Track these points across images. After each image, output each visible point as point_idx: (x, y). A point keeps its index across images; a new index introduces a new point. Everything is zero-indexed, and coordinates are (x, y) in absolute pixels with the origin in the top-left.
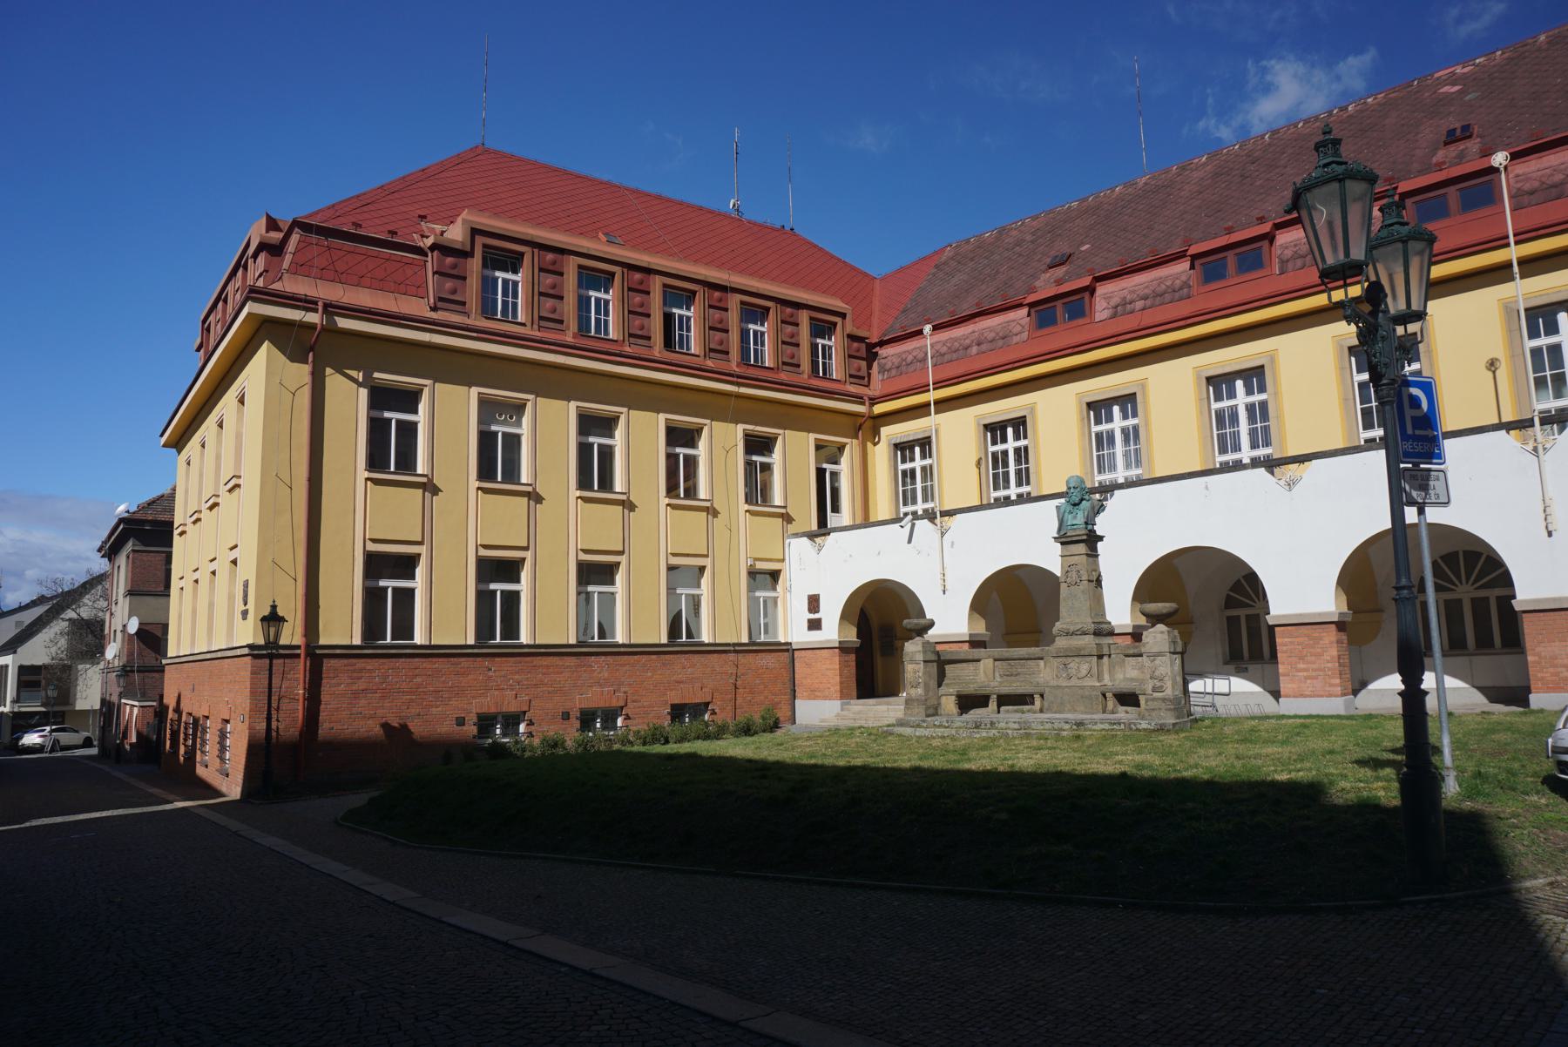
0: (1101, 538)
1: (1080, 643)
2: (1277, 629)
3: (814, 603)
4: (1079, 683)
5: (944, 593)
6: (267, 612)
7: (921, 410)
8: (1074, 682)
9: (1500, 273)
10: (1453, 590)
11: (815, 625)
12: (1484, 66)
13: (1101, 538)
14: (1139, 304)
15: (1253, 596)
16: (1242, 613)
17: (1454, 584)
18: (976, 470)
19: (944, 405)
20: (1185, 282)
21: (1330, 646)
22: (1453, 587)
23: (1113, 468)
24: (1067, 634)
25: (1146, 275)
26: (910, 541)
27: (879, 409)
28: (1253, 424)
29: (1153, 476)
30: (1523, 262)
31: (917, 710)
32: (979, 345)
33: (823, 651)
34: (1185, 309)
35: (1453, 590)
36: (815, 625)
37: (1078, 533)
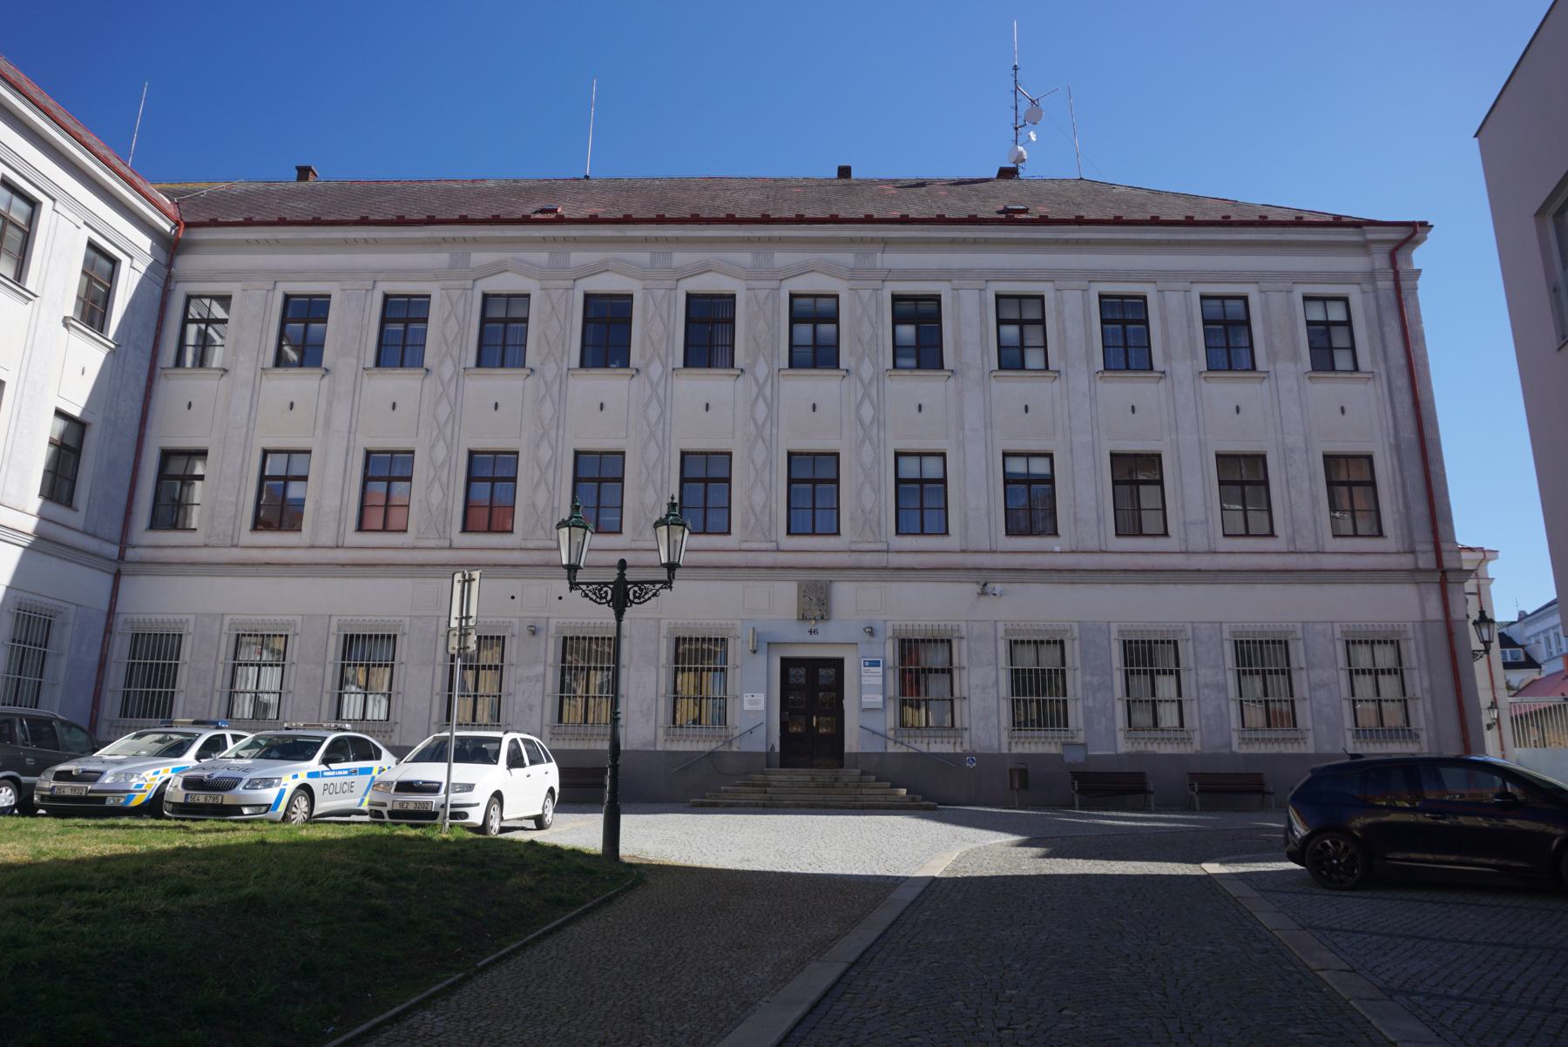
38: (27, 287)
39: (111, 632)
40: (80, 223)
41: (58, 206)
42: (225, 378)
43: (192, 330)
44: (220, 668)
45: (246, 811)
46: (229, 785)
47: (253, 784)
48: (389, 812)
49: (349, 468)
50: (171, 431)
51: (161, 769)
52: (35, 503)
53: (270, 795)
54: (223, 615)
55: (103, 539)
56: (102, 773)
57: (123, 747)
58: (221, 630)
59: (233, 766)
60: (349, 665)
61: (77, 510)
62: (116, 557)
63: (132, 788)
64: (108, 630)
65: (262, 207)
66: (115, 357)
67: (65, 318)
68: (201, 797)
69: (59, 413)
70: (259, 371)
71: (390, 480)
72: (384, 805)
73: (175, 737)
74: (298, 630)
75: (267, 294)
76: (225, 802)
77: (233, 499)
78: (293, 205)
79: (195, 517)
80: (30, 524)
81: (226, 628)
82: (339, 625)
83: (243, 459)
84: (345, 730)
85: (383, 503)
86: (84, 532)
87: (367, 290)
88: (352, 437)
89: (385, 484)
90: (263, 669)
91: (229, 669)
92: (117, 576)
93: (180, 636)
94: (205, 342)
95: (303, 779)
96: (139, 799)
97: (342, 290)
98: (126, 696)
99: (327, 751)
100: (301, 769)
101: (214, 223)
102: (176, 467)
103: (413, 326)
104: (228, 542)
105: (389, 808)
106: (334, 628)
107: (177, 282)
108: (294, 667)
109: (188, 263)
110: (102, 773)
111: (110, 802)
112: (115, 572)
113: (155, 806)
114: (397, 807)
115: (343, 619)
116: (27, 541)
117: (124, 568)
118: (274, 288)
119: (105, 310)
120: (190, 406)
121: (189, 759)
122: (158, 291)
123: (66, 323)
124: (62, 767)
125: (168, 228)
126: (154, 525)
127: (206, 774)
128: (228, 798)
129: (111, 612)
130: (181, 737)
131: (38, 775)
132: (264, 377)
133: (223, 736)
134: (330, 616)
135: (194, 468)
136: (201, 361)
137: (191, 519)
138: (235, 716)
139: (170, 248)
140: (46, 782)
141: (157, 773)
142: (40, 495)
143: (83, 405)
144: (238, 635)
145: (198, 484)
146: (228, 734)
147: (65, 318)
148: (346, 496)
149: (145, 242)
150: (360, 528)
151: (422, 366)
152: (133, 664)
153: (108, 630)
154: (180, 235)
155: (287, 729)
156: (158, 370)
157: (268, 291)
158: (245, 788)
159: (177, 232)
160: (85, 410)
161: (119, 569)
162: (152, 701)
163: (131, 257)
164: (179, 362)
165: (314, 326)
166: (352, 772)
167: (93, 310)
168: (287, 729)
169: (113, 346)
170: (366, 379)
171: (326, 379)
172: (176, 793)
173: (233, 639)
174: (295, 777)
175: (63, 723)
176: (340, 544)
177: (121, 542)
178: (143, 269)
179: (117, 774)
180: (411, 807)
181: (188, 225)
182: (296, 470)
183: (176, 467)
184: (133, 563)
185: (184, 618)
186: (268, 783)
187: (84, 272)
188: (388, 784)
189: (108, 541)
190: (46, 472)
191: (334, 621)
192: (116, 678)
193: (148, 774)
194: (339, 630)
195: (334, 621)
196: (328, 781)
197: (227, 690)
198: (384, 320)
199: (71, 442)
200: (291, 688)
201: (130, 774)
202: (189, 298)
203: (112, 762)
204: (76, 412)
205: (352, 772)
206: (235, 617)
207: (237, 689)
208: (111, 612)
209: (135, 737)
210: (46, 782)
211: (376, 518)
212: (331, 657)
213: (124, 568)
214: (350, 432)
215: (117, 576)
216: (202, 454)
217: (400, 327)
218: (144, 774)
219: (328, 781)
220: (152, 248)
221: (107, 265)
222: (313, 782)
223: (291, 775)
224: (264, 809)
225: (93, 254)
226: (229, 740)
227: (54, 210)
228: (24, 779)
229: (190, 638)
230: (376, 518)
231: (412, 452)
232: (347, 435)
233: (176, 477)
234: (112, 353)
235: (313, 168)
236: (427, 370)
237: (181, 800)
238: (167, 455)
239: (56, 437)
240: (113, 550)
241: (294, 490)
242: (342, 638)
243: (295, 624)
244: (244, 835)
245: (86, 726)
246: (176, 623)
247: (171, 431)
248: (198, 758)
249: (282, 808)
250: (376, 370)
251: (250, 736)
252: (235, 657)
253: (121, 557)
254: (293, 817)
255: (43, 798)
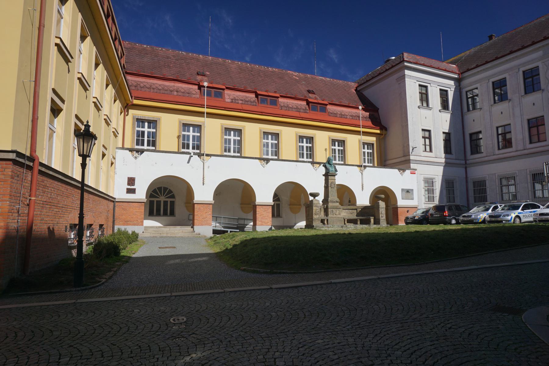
0: (323, 175)
1: (336, 205)
2: (257, 206)
3: (131, 181)
4: (336, 216)
5: (203, 185)
6: (117, 137)
7: (201, 114)
8: (335, 216)
9: (358, 133)
10: (159, 198)
11: (131, 191)
12: (184, 55)
13: (323, 175)
14: (240, 102)
15: (160, 195)
16: (155, 200)
17: (160, 196)
18: (177, 140)
19: (210, 115)
20: (254, 101)
21: (209, 210)
22: (159, 197)
23: (143, 144)
24: (332, 202)
25: (347, 109)
26: (188, 162)
27: (136, 102)
28: (142, 138)
29: (160, 150)
30: (207, 113)
31: (318, 222)
32: (177, 92)
33: (134, 204)
34: (297, 114)
35: (159, 198)
36: (131, 191)
37: (333, 173)
38: (430, 107)
39: (468, 182)
40: (437, 86)
41: (431, 85)
42: (481, 111)
43: (470, 100)
44: (497, 188)
45: (504, 222)
46: (499, 216)
47: (504, 216)
48: (538, 220)
49: (523, 126)
50: (472, 128)
51: (484, 214)
52: (443, 155)
53: (509, 218)
54: (495, 174)
55: (460, 160)
56: (472, 215)
57: (476, 209)
58: (495, 177)
59: (499, 212)
60: (535, 182)
61: (453, 154)
62: (464, 164)
63: (479, 218)
64: (467, 182)
65: (480, 57)
66: (452, 115)
67: (439, 110)
68: (493, 219)
69: (444, 133)
70: (490, 106)
71: (537, 126)
72: (537, 219)
73: (487, 207)
74: (518, 175)
75: (487, 84)
76: (499, 220)
77: (491, 142)
78: (489, 52)
79: (483, 149)
80: (443, 160)
81: (497, 177)
82: (530, 172)
83: (491, 131)
84: (528, 202)
85: (537, 133)
86: (456, 159)
87: (517, 72)
88: (522, 117)
89: (536, 128)
90: (510, 186)
91: (500, 187)
92: (466, 168)
93: (485, 181)
94: (474, 104)
95: (517, 214)
96: (480, 221)
97: (509, 75)
98: (475, 197)
99: (523, 207)
100: (516, 212)
101: (468, 70)
102: (474, 137)
103: (535, 78)
104: (492, 154)
105: (538, 219)
106: (528, 172)
107: (462, 89)
108: (518, 185)
109: (465, 82)
110: (472, 215)
111: (475, 221)
112: (465, 167)
113: (484, 221)
114: (540, 219)
115: (530, 169)
116: (444, 165)
117: (467, 166)
118: (489, 81)
119: (448, 104)
120: (474, 121)
121: (490, 211)
122: (458, 93)
123: (440, 111)
124: (463, 215)
125: (457, 77)
126: (472, 153)
127: (493, 214)
128: (499, 219)
129: (466, 177)
130: (488, 207)
131: (459, 217)
132: (492, 107)
133: (498, 206)
134: (527, 169)
135: (479, 137)
136: (474, 108)
137: (481, 150)
138: (504, 200)
139: (458, 81)
140: (461, 218)
141: (483, 215)
142: (444, 153)
143: (448, 129)
144: (500, 178)
145: (481, 140)
146: (499, 205)
147: (439, 110)
148: (524, 134)
149: (452, 83)
150: (531, 142)
151: (541, 89)
152: (475, 189)
153: (467, 182)
154: (460, 77)
155: (512, 203)
156: (464, 114)
157: (487, 83)
158: (503, 217)
159: (459, 76)
160: (449, 130)
161: (466, 166)
162: (483, 198)
163: (450, 88)
164: (468, 110)
165: (503, 88)
166: (531, 212)
167: (445, 106)
168: (512, 203)
169: (451, 112)
170: (523, 99)
171: (510, 102)
172: (488, 219)
173: (499, 179)
174: (515, 214)
175: (462, 206)
176: (525, 148)
177: (465, 159)
178: (453, 90)
179: (475, 215)
180: (544, 219)
181: (462, 73)
182: (507, 130)
183: (474, 137)
184: (469, 164)
185: (485, 176)
186: (508, 215)
187: (440, 97)
188: (537, 214)
189: (462, 160)
190: (444, 147)
191: (528, 170)
192: (471, 193)
193: (481, 215)
194: (530, 173)
195: (528, 170)
196: (524, 214)
197: (500, 193)
198: (525, 79)
199: (448, 138)
200: (519, 191)
201: (477, 215)
202: (467, 92)
203: (473, 213)
204: (447, 131)
205: (531, 212)
206: (499, 174)
207: (503, 193)
208: (466, 177)
209: (477, 207)
210: (461, 218)
211: (535, 138)
212: (529, 181)
213: (467, 166)
214: (521, 116)
215: (466, 168)
216: (480, 132)
217: (530, 79)
218: (480, 215)
219: (523, 214)
220: (454, 83)
221: (445, 93)
222: (520, 215)
223: (513, 214)
224: (508, 221)
225: (441, 92)
226: (499, 206)
227: (431, 86)
228: (457, 218)
229: (488, 181)
230: (535, 138)
231: (543, 116)
232: (520, 117)
233: (475, 140)
234: (452, 114)
235: (493, 34)
236: (543, 90)
237: (489, 220)
238: (471, 135)
239: (444, 138)
240: (463, 162)
241: (508, 136)
242: (532, 175)
243: (516, 173)
244: (501, 225)
245: (467, 206)
246: (481, 178)
247: (472, 128)
248: (492, 211)
249: (512, 221)
250: (525, 96)
251: (504, 205)
252: (501, 184)
253: (466, 163)
254: (516, 223)
255: (461, 221)
